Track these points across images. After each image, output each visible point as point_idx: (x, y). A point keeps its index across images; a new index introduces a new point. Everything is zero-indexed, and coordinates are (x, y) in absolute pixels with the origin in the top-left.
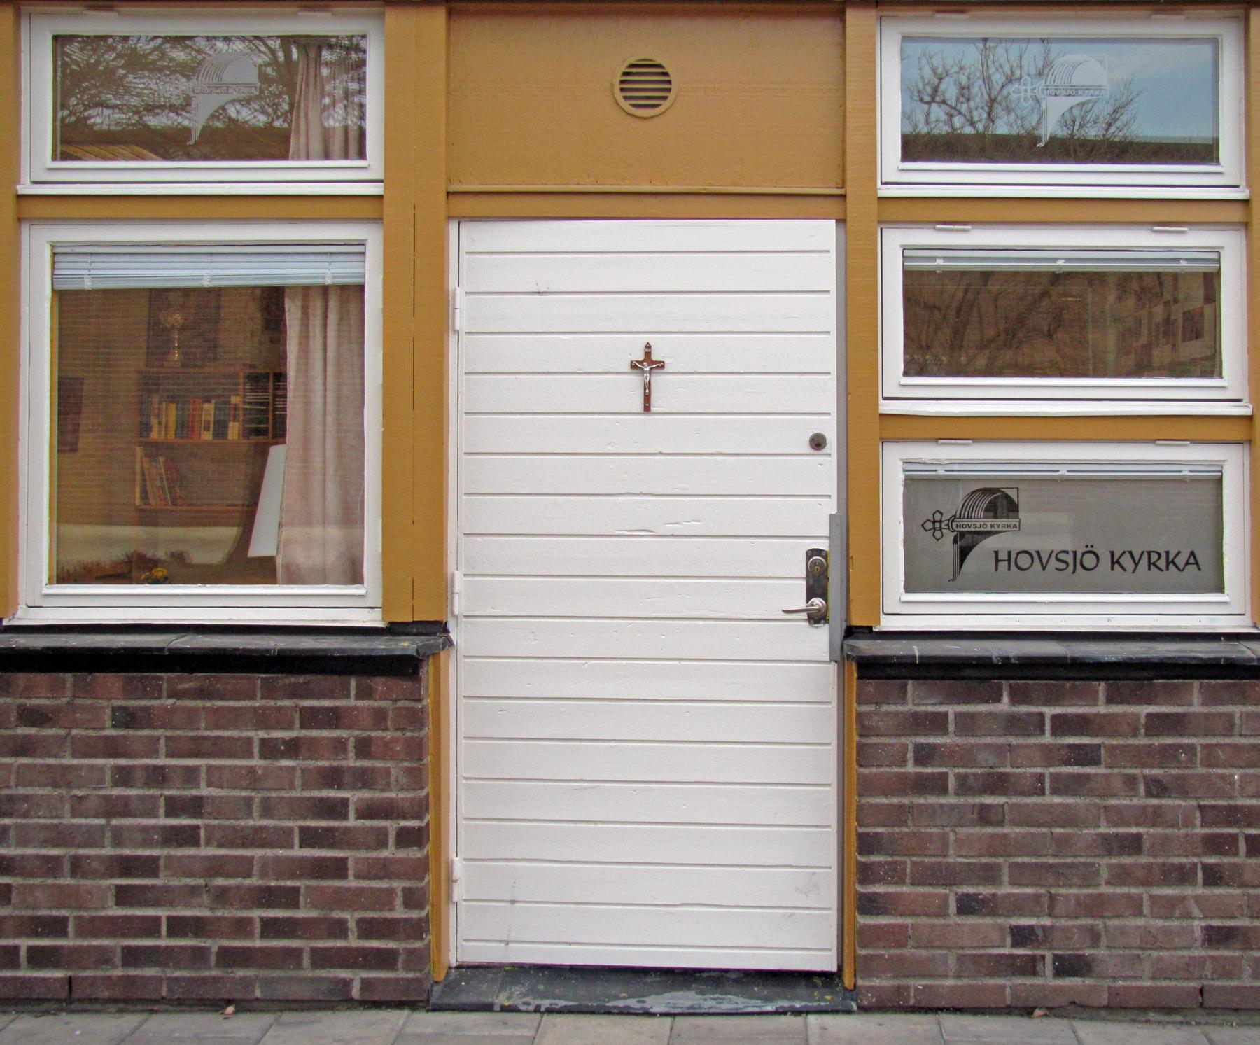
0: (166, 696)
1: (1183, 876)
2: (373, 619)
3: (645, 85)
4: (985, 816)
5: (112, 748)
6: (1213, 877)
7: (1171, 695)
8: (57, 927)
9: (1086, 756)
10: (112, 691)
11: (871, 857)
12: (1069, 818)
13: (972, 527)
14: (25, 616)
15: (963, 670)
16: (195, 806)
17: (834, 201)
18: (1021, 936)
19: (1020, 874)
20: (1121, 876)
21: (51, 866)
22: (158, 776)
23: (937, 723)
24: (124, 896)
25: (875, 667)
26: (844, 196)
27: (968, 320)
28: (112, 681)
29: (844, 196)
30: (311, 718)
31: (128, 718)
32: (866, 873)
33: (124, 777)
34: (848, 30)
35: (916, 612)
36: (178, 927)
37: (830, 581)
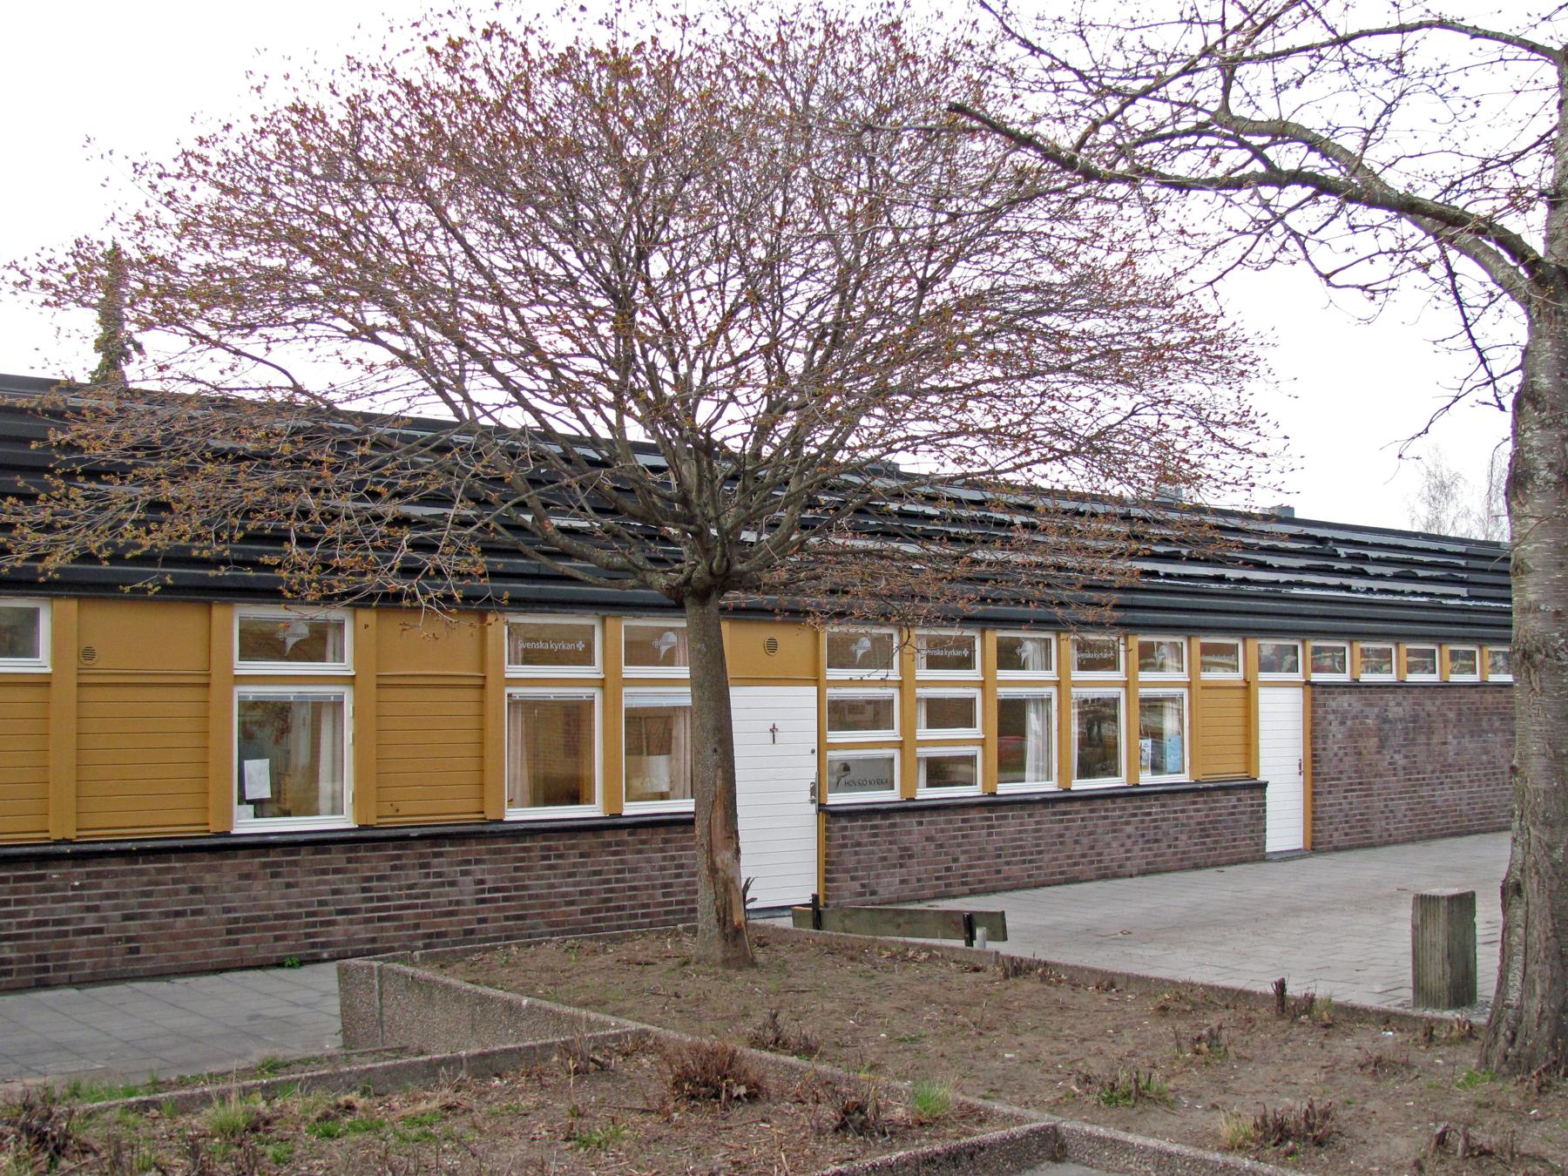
0: (1097, 804)
1: (894, 866)
2: (898, 798)
3: (772, 646)
4: (856, 853)
5: (662, 850)
6: (902, 866)
7: (551, 839)
8: (647, 906)
9: (875, 835)
10: (661, 834)
11: (829, 867)
12: (873, 853)
13: (846, 775)
14: (235, 831)
15: (853, 814)
16: (682, 866)
17: (816, 681)
18: (863, 886)
19: (864, 869)
20: (883, 867)
21: (647, 887)
22: (673, 858)
23: (845, 828)
24: (664, 895)
25: (829, 815)
26: (207, 685)
27: (841, 714)
28: (662, 830)
29: (207, 685)
30: (964, 821)
31: (665, 841)
32: (827, 871)
33: (664, 859)
34: (215, 622)
35: (835, 799)
36: (678, 903)
37: (817, 790)
